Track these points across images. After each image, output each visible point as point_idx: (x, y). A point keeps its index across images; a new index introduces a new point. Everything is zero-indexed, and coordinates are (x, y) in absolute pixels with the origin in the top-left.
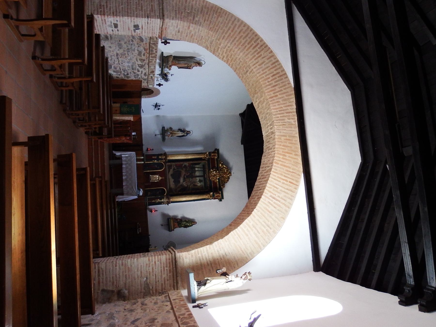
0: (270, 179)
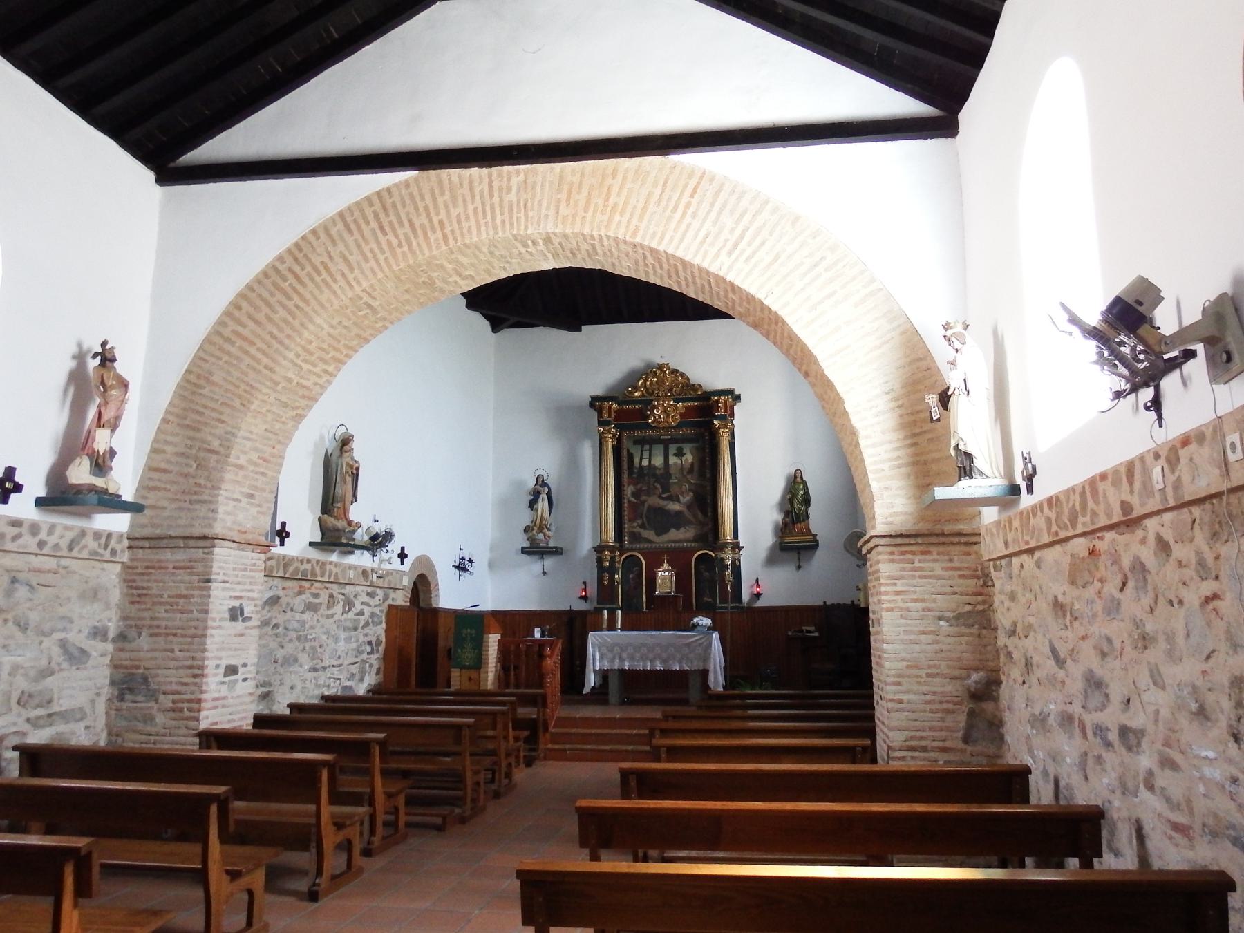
0: (679, 254)
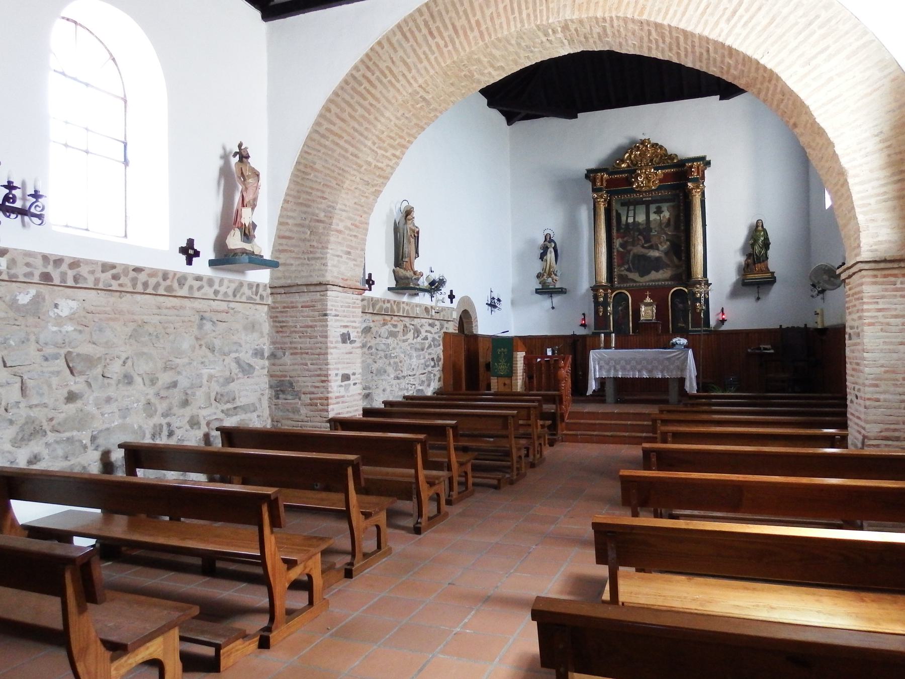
0: (682, 26)
